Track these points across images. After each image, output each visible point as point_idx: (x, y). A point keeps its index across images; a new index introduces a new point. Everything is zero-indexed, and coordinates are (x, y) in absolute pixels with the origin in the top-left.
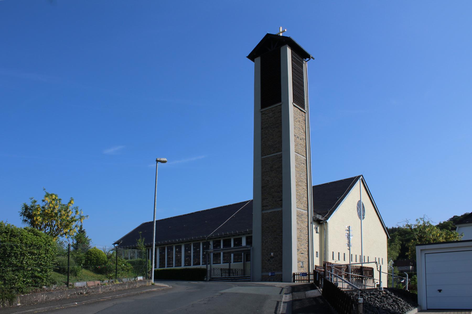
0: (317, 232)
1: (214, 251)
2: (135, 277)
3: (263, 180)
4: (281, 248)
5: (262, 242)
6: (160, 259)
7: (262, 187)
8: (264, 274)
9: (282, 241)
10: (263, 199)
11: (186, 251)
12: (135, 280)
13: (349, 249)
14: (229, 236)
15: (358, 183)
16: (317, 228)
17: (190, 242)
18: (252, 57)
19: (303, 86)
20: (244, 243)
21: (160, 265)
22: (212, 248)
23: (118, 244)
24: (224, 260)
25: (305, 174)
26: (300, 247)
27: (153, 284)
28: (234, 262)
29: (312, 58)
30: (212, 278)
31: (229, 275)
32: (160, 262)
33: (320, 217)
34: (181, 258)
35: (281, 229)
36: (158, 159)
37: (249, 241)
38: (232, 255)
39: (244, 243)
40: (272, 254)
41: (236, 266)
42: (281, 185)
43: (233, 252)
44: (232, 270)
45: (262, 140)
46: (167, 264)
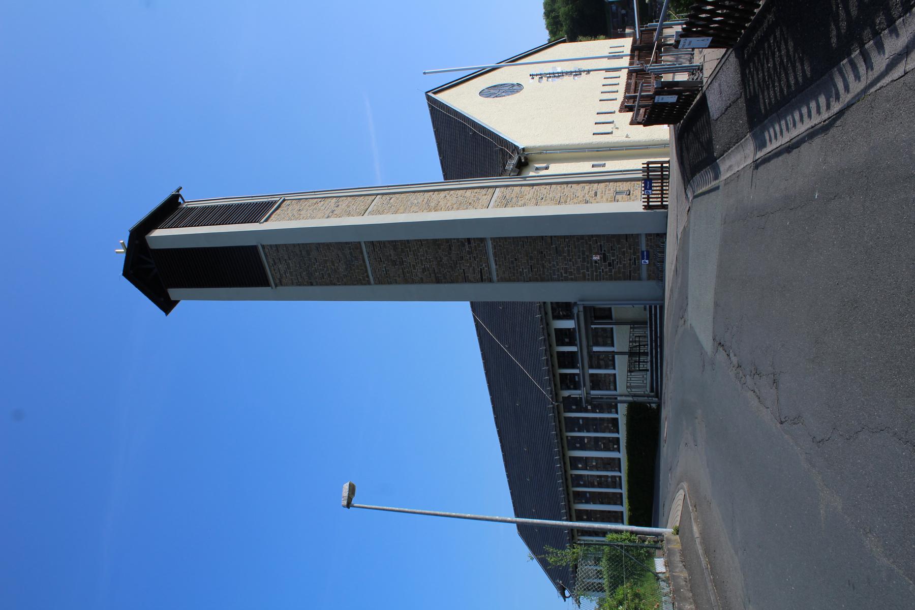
0: (547, 168)
1: (584, 385)
2: (658, 579)
3: (421, 281)
4: (582, 237)
5: (566, 279)
6: (602, 503)
7: (438, 281)
8: (644, 273)
9: (565, 237)
10: (466, 280)
11: (583, 448)
12: (667, 580)
13: (588, 72)
14: (551, 356)
15: (442, 97)
16: (537, 169)
17: (562, 439)
18: (167, 305)
19: (230, 206)
20: (569, 324)
21: (615, 504)
22: (579, 392)
23: (564, 589)
24: (606, 367)
25: (413, 196)
26: (580, 199)
27: (677, 532)
28: (613, 345)
29: (178, 191)
30: (652, 391)
31: (646, 354)
32: (609, 503)
33: (512, 163)
34: (601, 458)
35: (534, 239)
36: (345, 503)
37: (564, 310)
38: (595, 349)
39: (569, 324)
40: (596, 258)
41: (622, 339)
42: (435, 241)
43: (589, 347)
44: (631, 348)
45: (335, 284)
46: (615, 487)
